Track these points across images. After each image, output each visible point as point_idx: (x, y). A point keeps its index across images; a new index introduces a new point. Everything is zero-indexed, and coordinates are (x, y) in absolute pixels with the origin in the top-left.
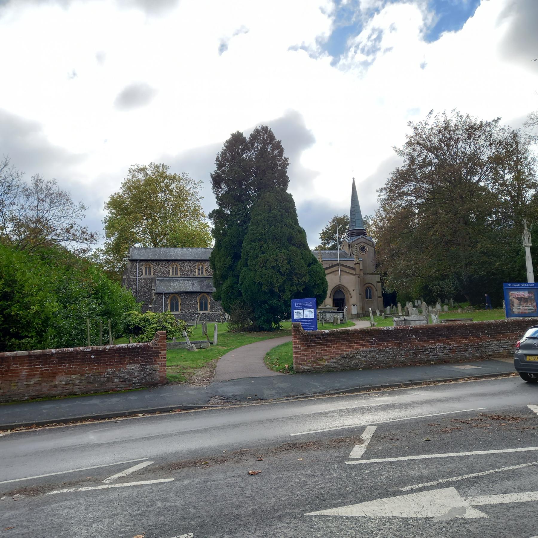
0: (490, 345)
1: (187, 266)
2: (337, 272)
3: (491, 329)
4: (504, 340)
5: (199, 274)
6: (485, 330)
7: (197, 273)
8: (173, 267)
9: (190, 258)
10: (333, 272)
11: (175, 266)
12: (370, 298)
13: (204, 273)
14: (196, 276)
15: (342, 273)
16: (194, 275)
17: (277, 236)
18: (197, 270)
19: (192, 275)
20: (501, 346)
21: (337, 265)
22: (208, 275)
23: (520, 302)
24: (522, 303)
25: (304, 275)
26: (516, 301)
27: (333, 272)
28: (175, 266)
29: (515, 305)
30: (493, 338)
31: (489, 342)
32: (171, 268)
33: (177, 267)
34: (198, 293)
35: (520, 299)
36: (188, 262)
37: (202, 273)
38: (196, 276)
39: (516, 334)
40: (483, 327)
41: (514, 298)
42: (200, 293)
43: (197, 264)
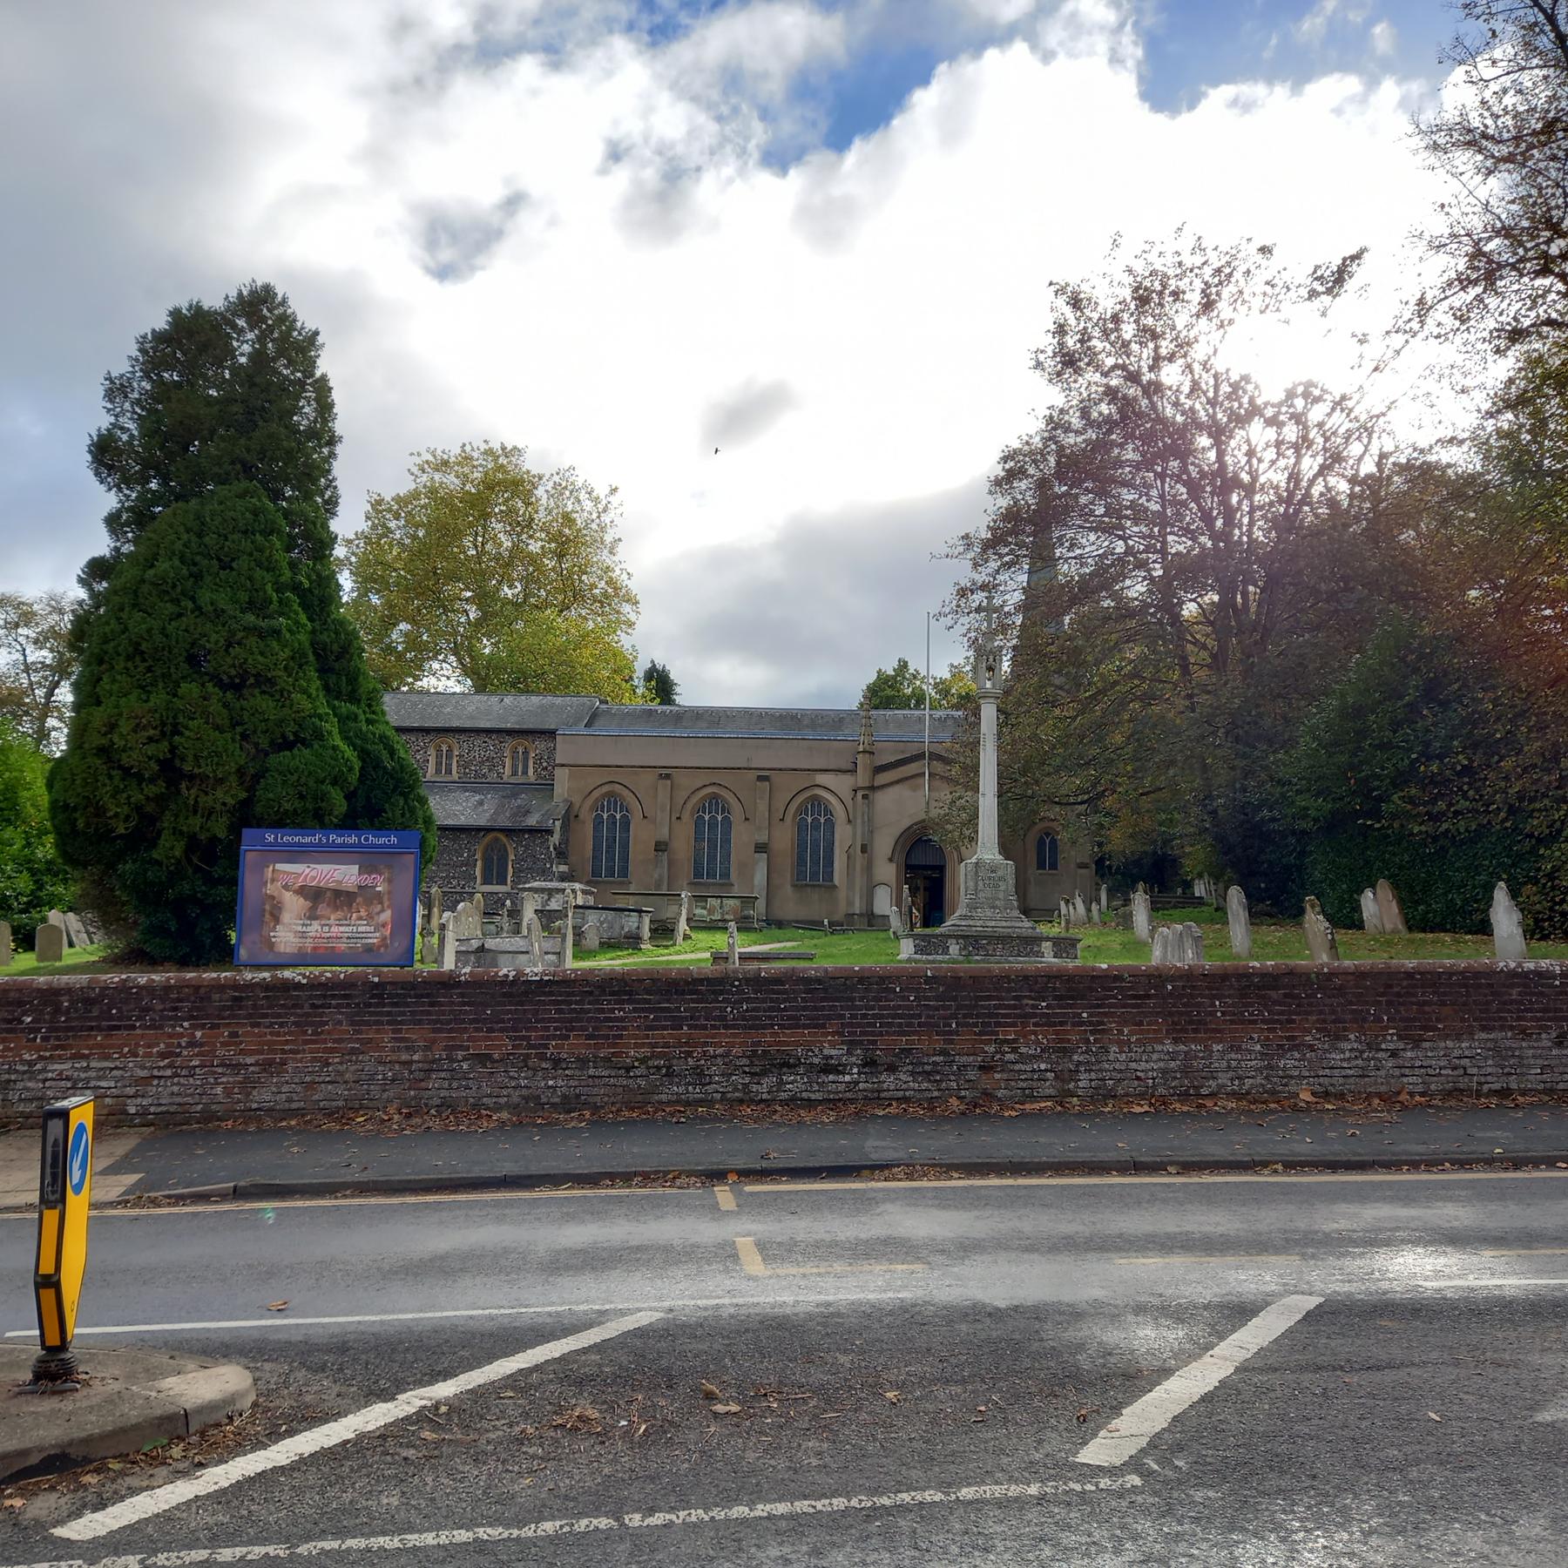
0: (31, 1074)
1: (480, 749)
2: (919, 780)
3: (57, 1010)
4: (107, 1057)
5: (514, 773)
6: (25, 1014)
7: (508, 771)
8: (439, 750)
9: (488, 725)
10: (907, 779)
11: (444, 748)
12: (1054, 866)
13: (531, 771)
14: (505, 779)
15: (937, 783)
16: (500, 776)
17: (144, 646)
18: (508, 762)
19: (493, 777)
20: (88, 1080)
21: (921, 756)
22: (539, 776)
23: (313, 908)
24: (322, 909)
25: (221, 781)
26: (293, 904)
27: (907, 779)
28: (444, 748)
29: (286, 917)
30: (56, 1048)
31: (31, 1063)
32: (432, 752)
33: (450, 750)
34: (479, 829)
35: (315, 895)
36: (483, 737)
37: (525, 772)
38: (505, 779)
39: (170, 1036)
40: (20, 1003)
41: (286, 887)
42: (488, 830)
43: (509, 743)
